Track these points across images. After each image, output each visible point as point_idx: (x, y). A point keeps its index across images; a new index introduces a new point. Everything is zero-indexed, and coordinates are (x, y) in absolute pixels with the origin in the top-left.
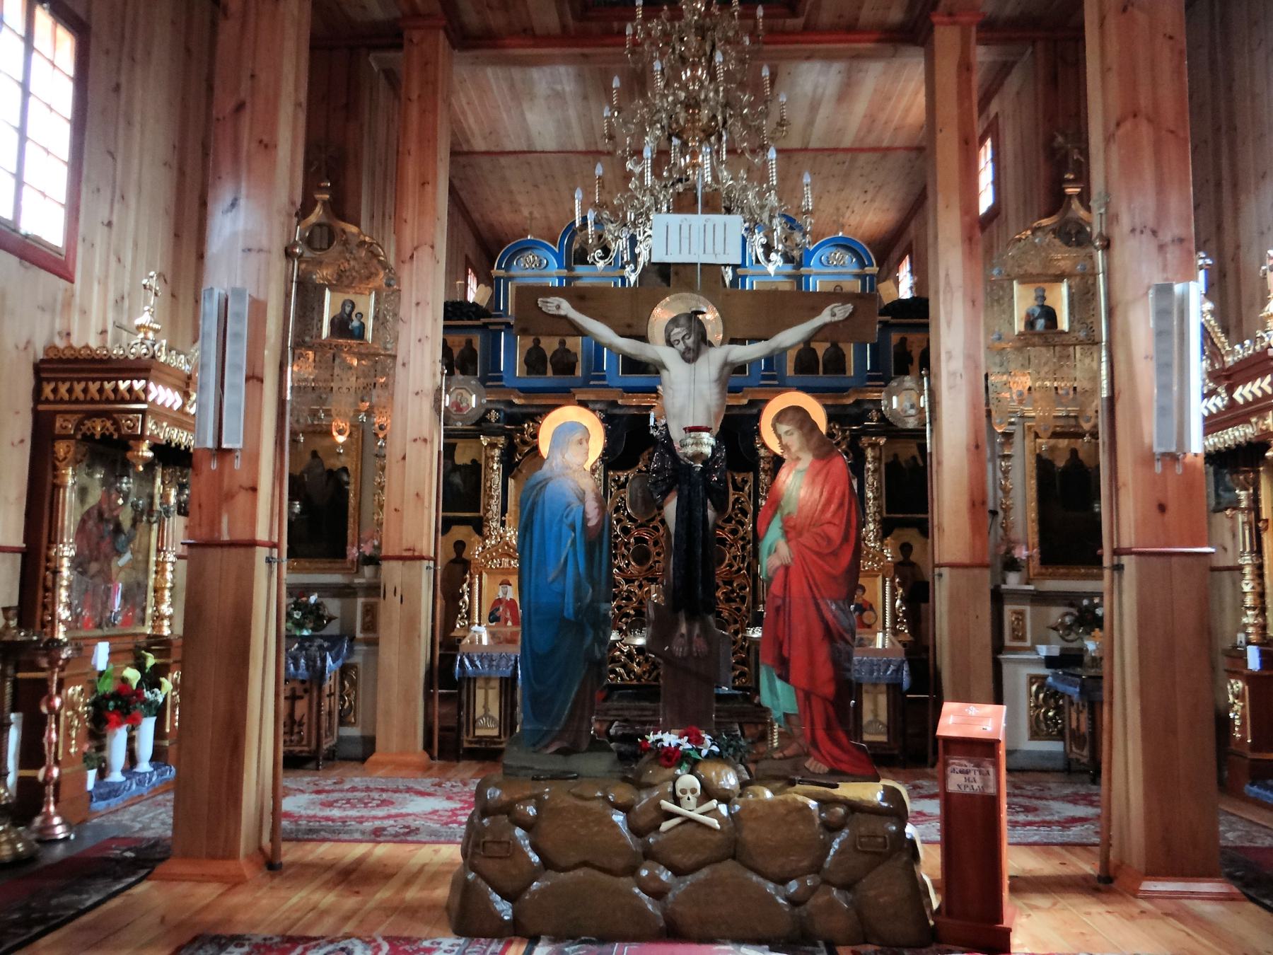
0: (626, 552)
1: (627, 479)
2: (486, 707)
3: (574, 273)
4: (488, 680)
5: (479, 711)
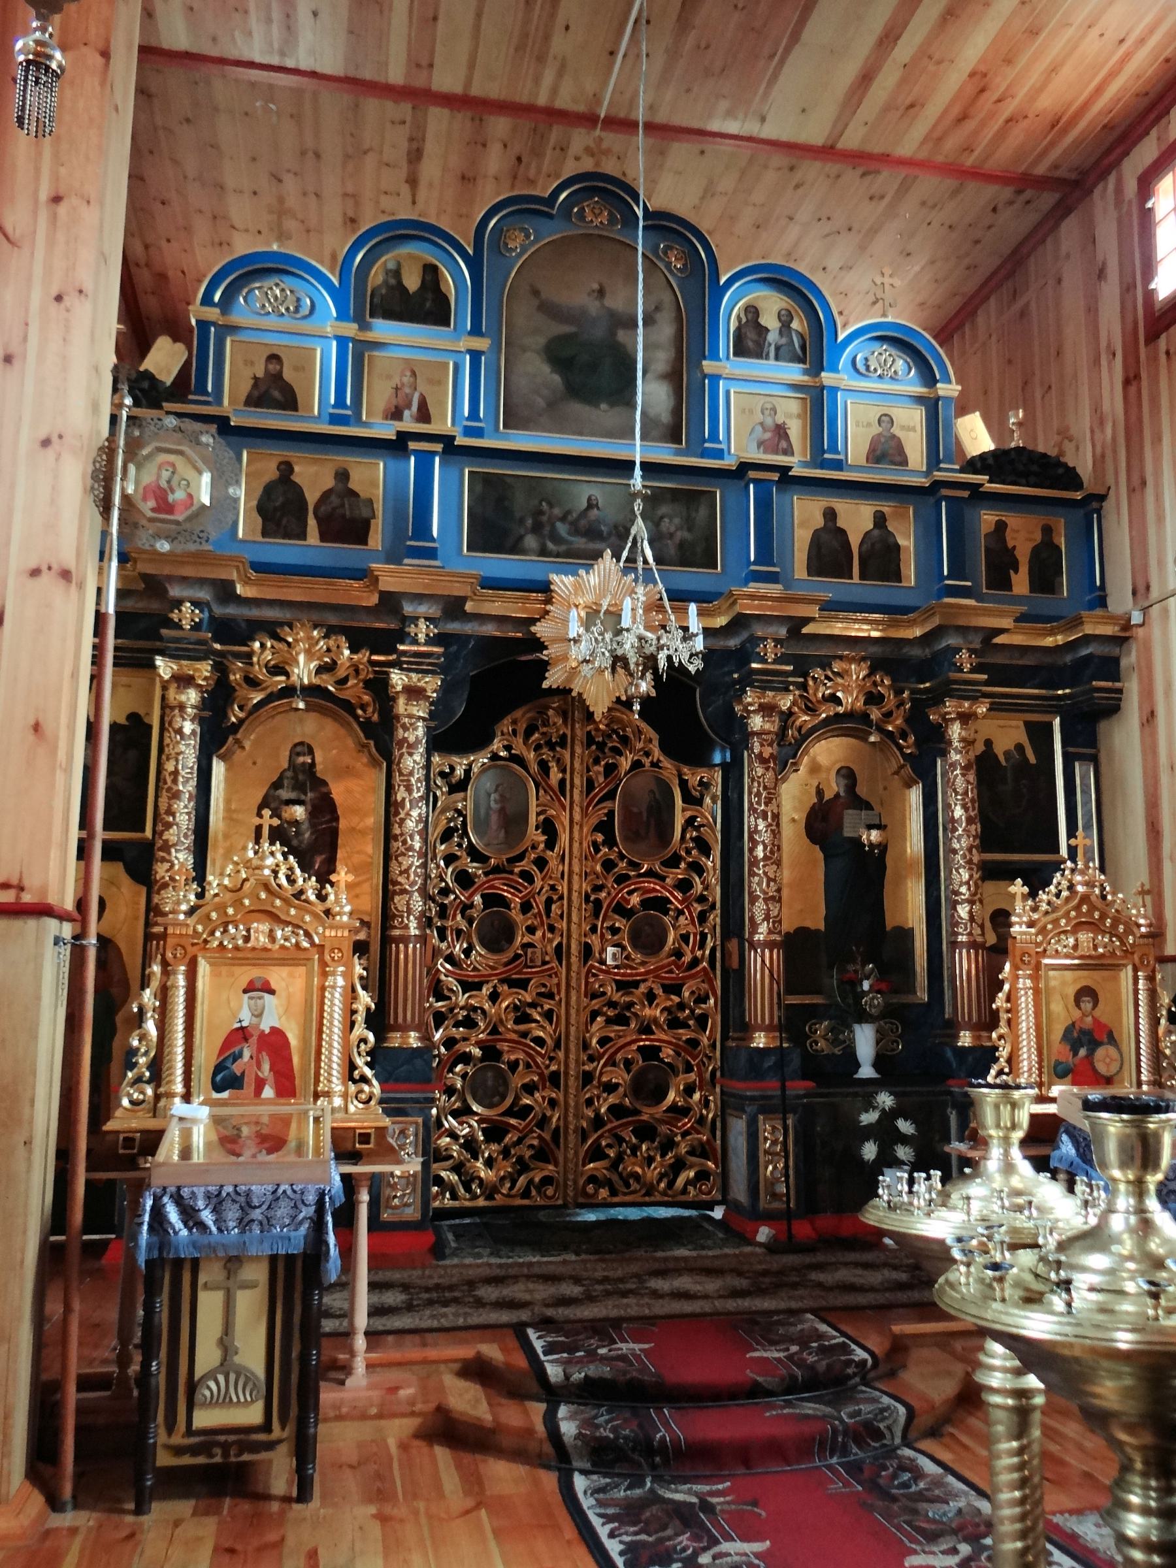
0: (464, 926)
1: (468, 772)
2: (226, 1344)
3: (370, 336)
4: (233, 1262)
5: (207, 1356)
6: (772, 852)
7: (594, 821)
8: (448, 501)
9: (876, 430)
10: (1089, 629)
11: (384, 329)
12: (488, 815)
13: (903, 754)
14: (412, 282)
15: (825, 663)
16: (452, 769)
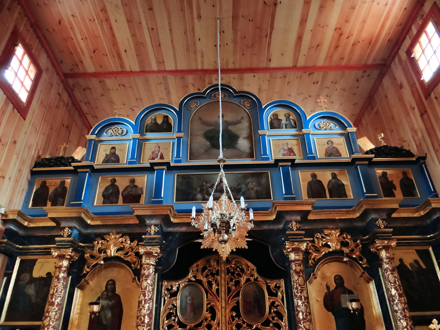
1: (178, 288)
6: (306, 316)
7: (231, 307)
8: (169, 184)
9: (327, 146)
10: (434, 205)
11: (149, 135)
13: (362, 267)
14: (160, 121)
15: (321, 231)
16: (172, 287)
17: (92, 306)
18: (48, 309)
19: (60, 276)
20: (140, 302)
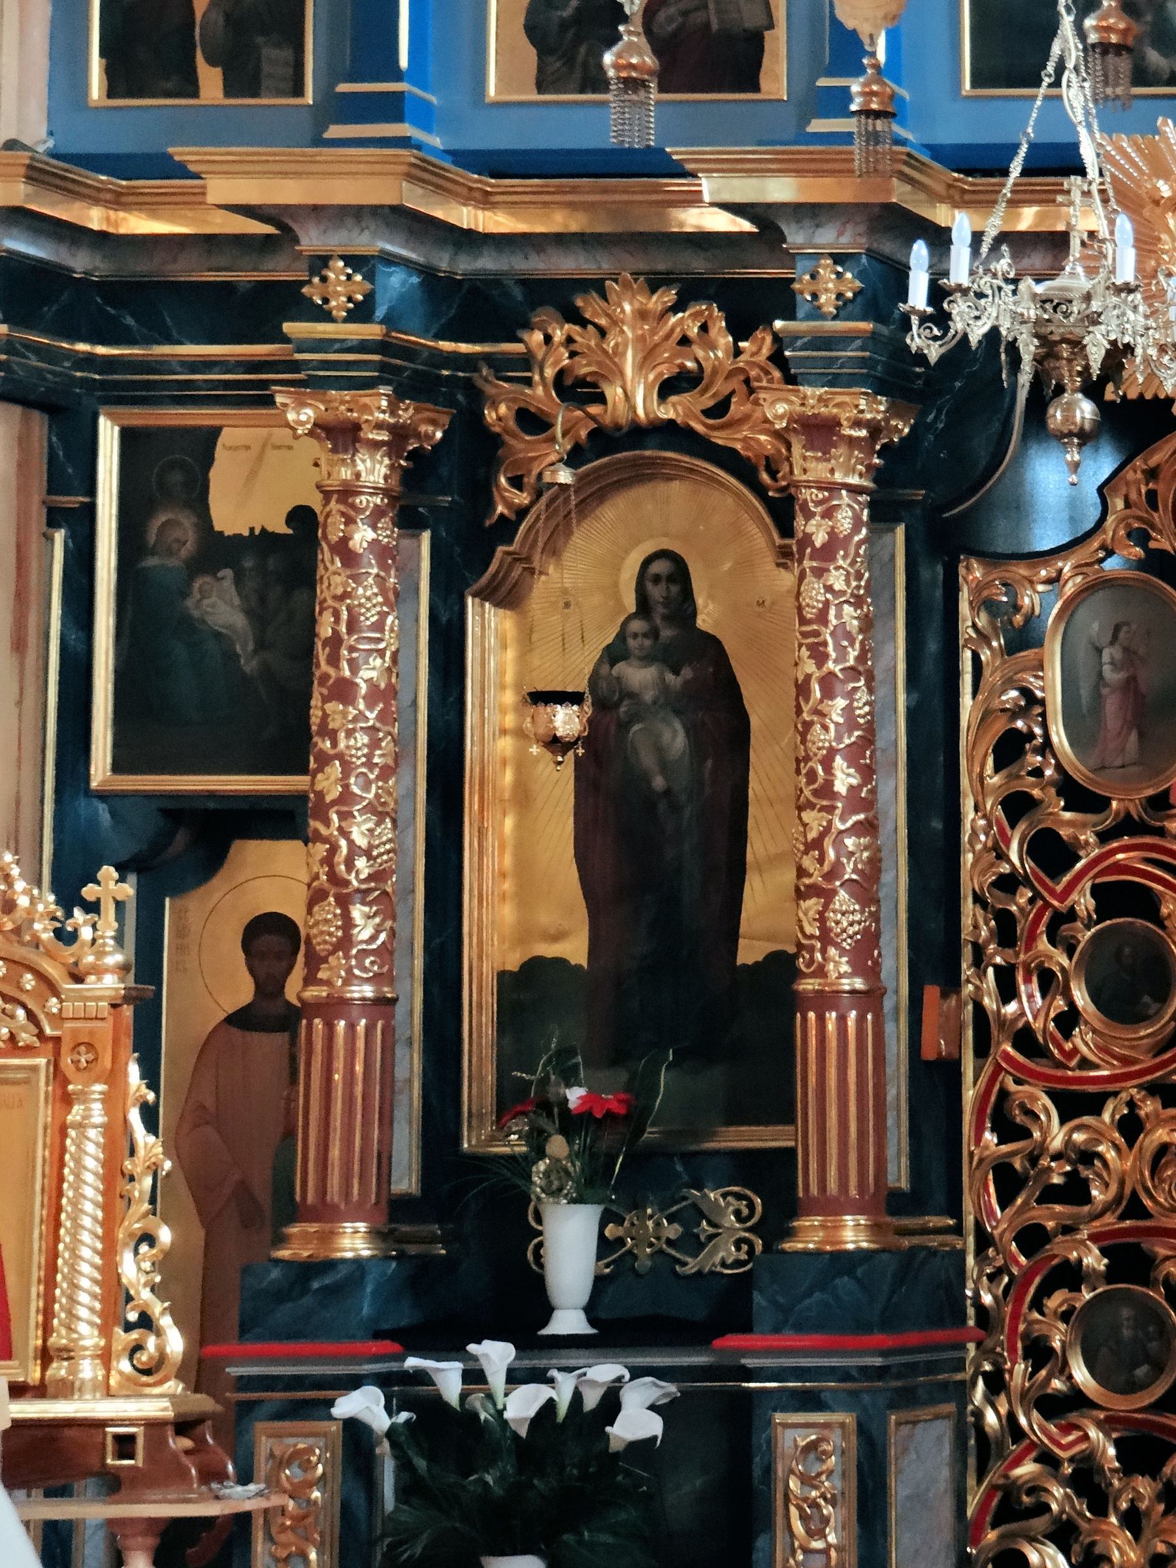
12: (1098, 698)
17: (543, 710)
18: (325, 716)
19: (357, 537)
20: (803, 689)
